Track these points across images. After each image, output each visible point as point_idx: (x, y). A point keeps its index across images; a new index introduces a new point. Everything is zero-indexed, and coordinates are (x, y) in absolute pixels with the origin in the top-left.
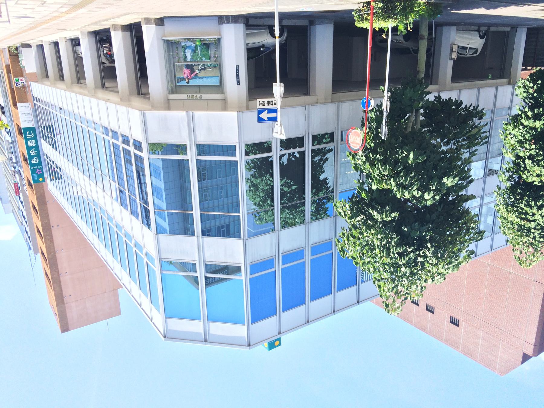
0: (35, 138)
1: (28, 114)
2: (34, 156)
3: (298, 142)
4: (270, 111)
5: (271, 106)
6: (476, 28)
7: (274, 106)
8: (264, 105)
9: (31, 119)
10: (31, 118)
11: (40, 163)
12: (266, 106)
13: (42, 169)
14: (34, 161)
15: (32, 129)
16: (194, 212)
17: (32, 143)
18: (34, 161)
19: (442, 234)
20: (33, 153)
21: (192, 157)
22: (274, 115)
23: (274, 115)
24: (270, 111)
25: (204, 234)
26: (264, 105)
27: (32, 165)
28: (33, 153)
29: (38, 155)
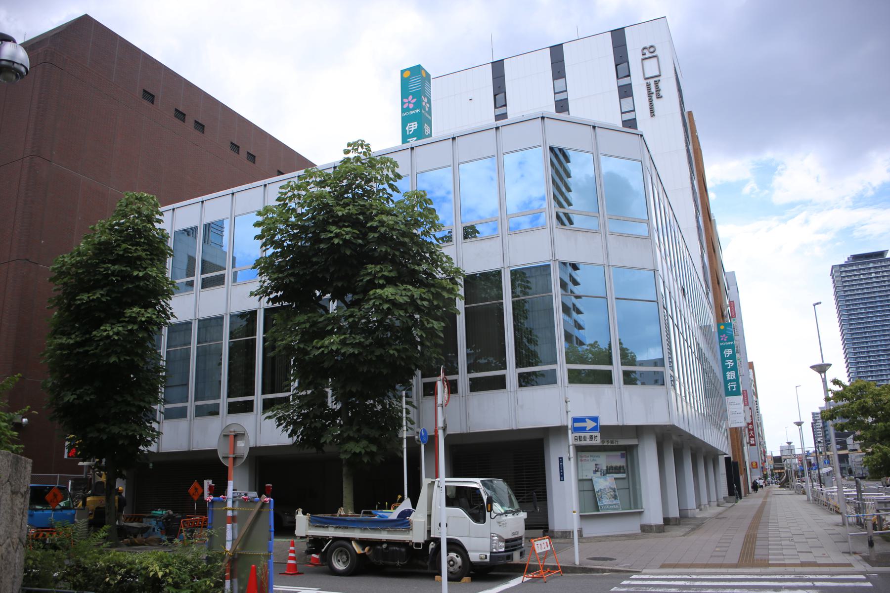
0: (726, 382)
1: (733, 413)
2: (729, 358)
3: (201, 412)
4: (583, 429)
5: (582, 435)
6: (674, 513)
7: (578, 435)
8: (591, 437)
9: (732, 407)
10: (731, 409)
11: (722, 349)
12: (588, 435)
13: (720, 341)
14: (729, 352)
15: (729, 393)
16: (504, 301)
17: (731, 375)
18: (729, 352)
19: (166, 291)
20: (730, 363)
21: (511, 372)
22: (577, 425)
23: (577, 425)
24: (583, 429)
25: (498, 273)
26: (591, 437)
27: (732, 347)
28: (730, 363)
29: (724, 359)
